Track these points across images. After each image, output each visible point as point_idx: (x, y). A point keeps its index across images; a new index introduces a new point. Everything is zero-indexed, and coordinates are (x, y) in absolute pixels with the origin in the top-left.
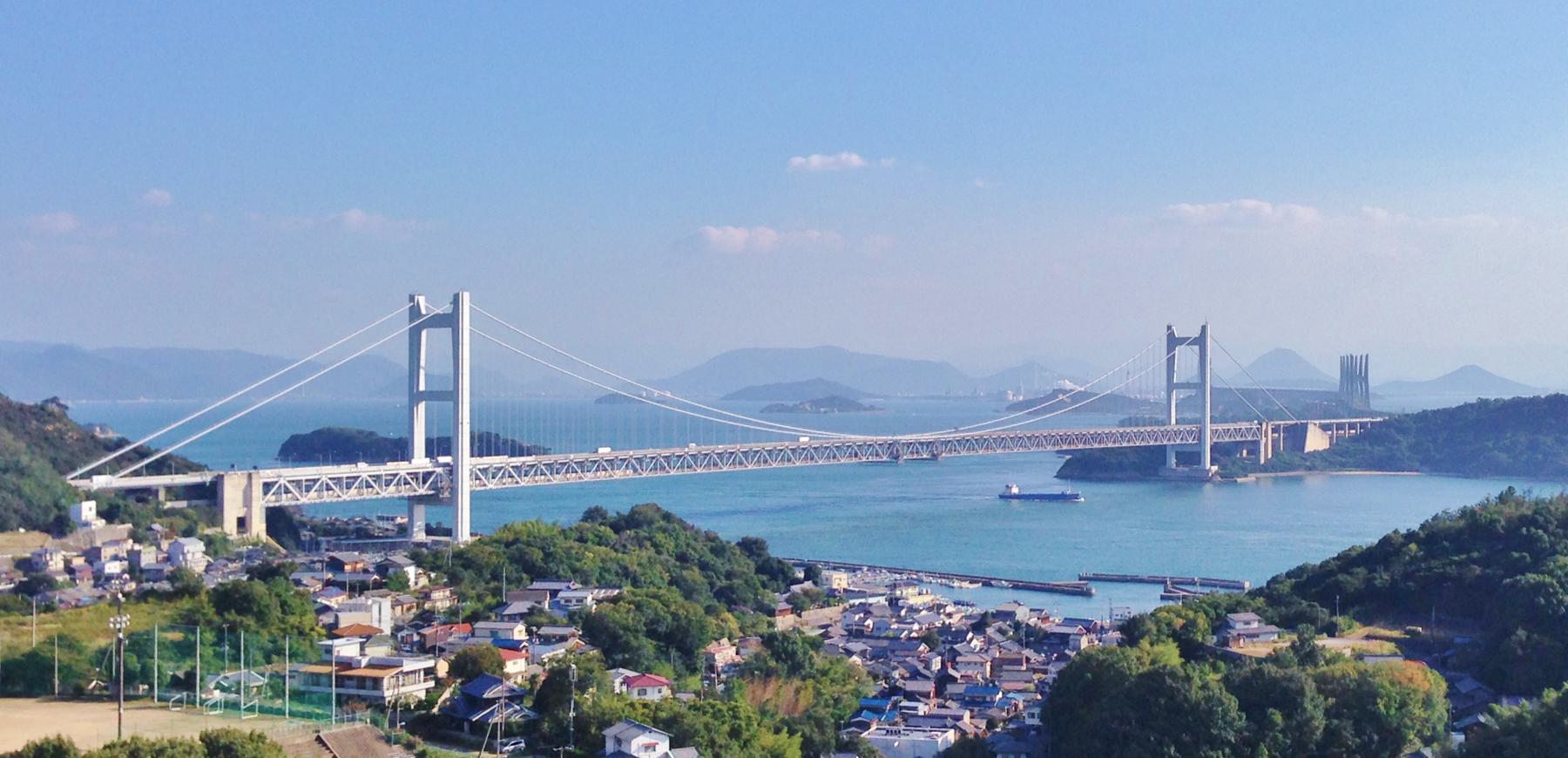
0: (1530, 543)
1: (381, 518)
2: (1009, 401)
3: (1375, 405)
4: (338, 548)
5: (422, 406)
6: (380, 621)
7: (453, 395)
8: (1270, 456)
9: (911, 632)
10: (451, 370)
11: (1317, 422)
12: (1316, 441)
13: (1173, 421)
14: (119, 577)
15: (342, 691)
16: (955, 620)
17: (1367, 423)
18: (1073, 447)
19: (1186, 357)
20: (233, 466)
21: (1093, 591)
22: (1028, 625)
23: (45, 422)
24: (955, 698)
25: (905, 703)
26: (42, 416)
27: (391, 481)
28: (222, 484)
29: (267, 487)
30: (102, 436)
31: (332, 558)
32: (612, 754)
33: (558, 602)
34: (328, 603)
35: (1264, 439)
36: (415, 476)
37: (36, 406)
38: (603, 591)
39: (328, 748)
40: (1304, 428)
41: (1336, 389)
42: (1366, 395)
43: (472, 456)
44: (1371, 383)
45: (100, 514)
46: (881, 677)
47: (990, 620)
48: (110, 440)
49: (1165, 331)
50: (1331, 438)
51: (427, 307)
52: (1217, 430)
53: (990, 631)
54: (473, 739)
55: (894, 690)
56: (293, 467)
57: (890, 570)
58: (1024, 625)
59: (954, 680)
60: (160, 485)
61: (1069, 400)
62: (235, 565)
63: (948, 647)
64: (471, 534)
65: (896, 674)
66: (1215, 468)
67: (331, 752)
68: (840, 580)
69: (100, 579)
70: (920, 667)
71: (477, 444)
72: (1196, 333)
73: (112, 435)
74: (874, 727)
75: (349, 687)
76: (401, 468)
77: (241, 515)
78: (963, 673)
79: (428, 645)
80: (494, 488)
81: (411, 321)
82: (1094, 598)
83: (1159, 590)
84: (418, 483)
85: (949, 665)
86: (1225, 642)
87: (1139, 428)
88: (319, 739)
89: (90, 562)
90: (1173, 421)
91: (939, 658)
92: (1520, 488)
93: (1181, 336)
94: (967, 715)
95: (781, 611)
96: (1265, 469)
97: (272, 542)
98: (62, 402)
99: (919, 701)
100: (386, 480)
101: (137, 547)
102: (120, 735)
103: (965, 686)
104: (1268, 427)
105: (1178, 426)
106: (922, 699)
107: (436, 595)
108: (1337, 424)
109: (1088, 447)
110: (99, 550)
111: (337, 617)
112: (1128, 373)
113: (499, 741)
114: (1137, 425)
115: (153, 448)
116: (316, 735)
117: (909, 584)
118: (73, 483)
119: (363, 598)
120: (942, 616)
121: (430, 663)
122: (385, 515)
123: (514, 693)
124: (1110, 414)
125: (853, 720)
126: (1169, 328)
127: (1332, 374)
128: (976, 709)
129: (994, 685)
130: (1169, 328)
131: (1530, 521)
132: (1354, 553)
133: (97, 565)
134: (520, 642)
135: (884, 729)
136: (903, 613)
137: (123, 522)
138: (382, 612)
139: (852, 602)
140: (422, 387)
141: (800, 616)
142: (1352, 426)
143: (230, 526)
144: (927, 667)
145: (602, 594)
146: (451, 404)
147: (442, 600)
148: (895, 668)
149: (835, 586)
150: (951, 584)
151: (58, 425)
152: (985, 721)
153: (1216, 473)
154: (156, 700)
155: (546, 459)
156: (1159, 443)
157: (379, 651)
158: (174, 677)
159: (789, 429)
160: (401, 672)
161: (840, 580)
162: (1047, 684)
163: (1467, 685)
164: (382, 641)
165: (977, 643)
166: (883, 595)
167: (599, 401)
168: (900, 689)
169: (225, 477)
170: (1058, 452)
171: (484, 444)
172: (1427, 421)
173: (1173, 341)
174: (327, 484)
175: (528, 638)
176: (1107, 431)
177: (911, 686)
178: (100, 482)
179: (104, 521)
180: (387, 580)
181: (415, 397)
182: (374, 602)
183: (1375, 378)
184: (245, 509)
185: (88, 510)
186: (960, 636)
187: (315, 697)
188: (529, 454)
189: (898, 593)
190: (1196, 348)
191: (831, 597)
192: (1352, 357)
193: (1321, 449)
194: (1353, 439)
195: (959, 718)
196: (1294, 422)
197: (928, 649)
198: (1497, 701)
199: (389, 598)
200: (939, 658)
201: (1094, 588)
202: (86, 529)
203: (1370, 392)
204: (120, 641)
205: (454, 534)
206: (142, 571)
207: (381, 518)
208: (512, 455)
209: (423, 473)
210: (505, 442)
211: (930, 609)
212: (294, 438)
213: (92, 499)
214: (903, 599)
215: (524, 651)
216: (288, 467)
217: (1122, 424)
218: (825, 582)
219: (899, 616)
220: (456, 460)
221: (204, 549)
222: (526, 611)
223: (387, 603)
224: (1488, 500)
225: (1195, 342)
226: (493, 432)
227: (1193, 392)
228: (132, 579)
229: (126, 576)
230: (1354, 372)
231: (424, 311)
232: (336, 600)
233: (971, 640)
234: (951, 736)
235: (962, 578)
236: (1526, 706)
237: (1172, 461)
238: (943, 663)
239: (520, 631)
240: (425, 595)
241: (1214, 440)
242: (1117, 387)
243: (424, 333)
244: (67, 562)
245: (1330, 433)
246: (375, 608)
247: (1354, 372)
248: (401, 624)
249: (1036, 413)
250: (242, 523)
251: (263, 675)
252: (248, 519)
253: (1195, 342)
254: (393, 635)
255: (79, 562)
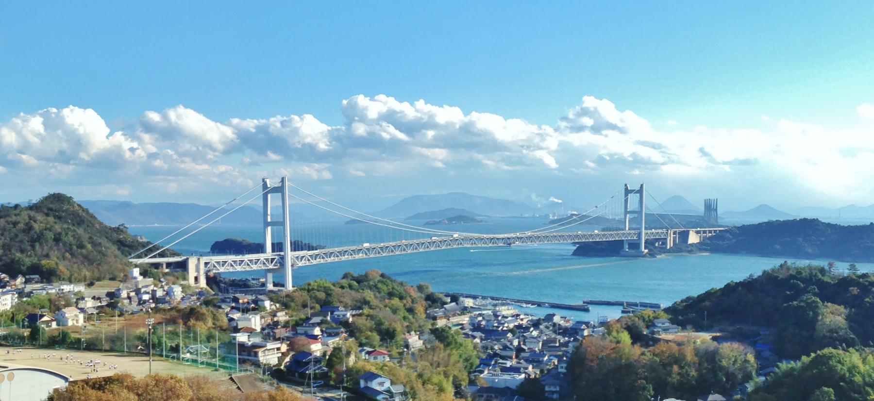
0: (794, 287)
1: (253, 279)
2: (550, 219)
3: (720, 222)
4: (236, 292)
5: (269, 228)
6: (255, 325)
7: (283, 224)
8: (672, 245)
9: (503, 327)
10: (282, 211)
11: (694, 230)
12: (693, 238)
13: (627, 229)
14: (148, 301)
15: (241, 357)
16: (524, 322)
17: (716, 230)
18: (580, 241)
19: (633, 199)
20: (192, 254)
21: (590, 308)
22: (559, 325)
23: (120, 234)
24: (523, 358)
25: (501, 361)
26: (118, 232)
27: (257, 262)
28: (188, 262)
29: (206, 264)
30: (141, 240)
31: (234, 297)
32: (363, 388)
33: (334, 317)
34: (233, 317)
35: (669, 237)
36: (267, 260)
37: (116, 228)
38: (354, 311)
39: (235, 383)
40: (688, 232)
41: (703, 215)
42: (716, 218)
43: (291, 251)
44: (718, 213)
45: (141, 274)
46: (489, 348)
47: (541, 322)
48: (145, 242)
49: (624, 187)
50: (700, 237)
51: (270, 184)
52: (647, 233)
53: (541, 327)
54: (300, 380)
55: (496, 355)
56: (217, 256)
57: (493, 299)
58: (557, 325)
59: (524, 350)
60: (164, 262)
61: (578, 219)
62: (194, 297)
63: (521, 334)
64: (293, 287)
65: (496, 347)
66: (646, 251)
67: (237, 385)
68: (469, 302)
69: (141, 302)
70: (508, 344)
71: (293, 246)
72: (638, 188)
73: (145, 240)
74: (486, 372)
75: (244, 355)
76: (261, 256)
77: (195, 275)
78: (528, 347)
79: (277, 337)
80: (301, 265)
81: (263, 190)
82: (591, 312)
83: (621, 308)
84: (268, 263)
85: (522, 343)
86: (653, 333)
87: (611, 232)
88: (231, 379)
89: (137, 294)
90: (627, 229)
91: (517, 340)
92: (790, 262)
93: (631, 189)
94: (530, 367)
95: (440, 317)
96: (669, 251)
97: (208, 288)
98: (126, 226)
99: (507, 360)
100: (255, 262)
101: (155, 289)
102: (150, 373)
103: (529, 353)
104: (671, 232)
105: (629, 231)
106: (509, 359)
107: (279, 314)
108: (703, 231)
109: (587, 241)
110: (140, 289)
111: (237, 323)
112: (606, 207)
113: (312, 381)
114: (610, 231)
115: (161, 245)
116: (230, 377)
117: (503, 305)
118: (130, 260)
119: (248, 315)
120: (518, 320)
121: (279, 345)
122: (255, 278)
123: (317, 360)
124: (597, 226)
125: (477, 369)
126: (626, 185)
127: (701, 209)
128: (535, 364)
129: (543, 353)
130: (626, 185)
131: (792, 277)
132: (713, 291)
133: (139, 296)
134: (318, 336)
135: (491, 373)
136: (500, 318)
137: (150, 277)
138: (256, 322)
139: (475, 313)
140: (269, 220)
141: (448, 320)
142: (710, 232)
143: (192, 281)
144: (511, 344)
145: (354, 312)
146: (282, 227)
147: (281, 316)
148: (495, 345)
149: (466, 306)
150: (522, 305)
151: (124, 235)
152: (539, 370)
153: (647, 253)
154: (164, 357)
155: (324, 251)
156: (620, 239)
157: (257, 340)
158: (171, 346)
159: (451, 233)
160: (267, 349)
161: (469, 302)
162: (569, 352)
163: (767, 354)
164: (257, 334)
165: (535, 333)
166: (490, 310)
167: (347, 223)
168: (498, 354)
169: (189, 259)
170: (573, 243)
171: (296, 246)
172: (745, 230)
173: (627, 192)
174: (231, 264)
175: (321, 334)
176: (597, 234)
177: (504, 353)
178: (139, 261)
179: (142, 277)
180: (256, 307)
181: (267, 224)
182: (253, 317)
183: (720, 211)
184: (197, 273)
185: (136, 272)
186: (527, 329)
187: (229, 359)
188: (316, 249)
189: (497, 309)
190: (638, 195)
191: (465, 310)
192: (710, 199)
193: (695, 242)
194: (710, 238)
195: (527, 368)
196: (683, 230)
197: (512, 335)
198: (780, 361)
199: (259, 315)
200: (517, 340)
201: (591, 307)
202: (135, 281)
203: (718, 216)
204: (150, 329)
205: (285, 286)
206: (157, 299)
207: (253, 279)
208: (309, 250)
209: (271, 259)
210: (305, 244)
211: (513, 316)
212: (217, 243)
213: (138, 267)
214: (499, 311)
215: (320, 340)
216: (214, 256)
217: (603, 230)
218: (461, 303)
219: (498, 320)
220: (285, 253)
221: (181, 290)
222: (320, 321)
223: (258, 317)
224: (775, 266)
225: (638, 192)
226: (300, 240)
227: (636, 215)
228: (153, 302)
229: (151, 301)
230: (710, 207)
231: (269, 186)
232: (236, 316)
233: (532, 331)
234: (523, 376)
235: (527, 302)
236: (792, 364)
237: (626, 246)
238: (519, 342)
239: (318, 331)
240: (274, 314)
241: (646, 238)
242: (599, 213)
243: (269, 195)
244: (128, 294)
245: (700, 235)
246: (253, 320)
247: (710, 207)
248: (264, 327)
249: (563, 225)
250: (196, 279)
251: (207, 348)
252: (198, 277)
253: (638, 192)
254: (261, 332)
255: (132, 294)
